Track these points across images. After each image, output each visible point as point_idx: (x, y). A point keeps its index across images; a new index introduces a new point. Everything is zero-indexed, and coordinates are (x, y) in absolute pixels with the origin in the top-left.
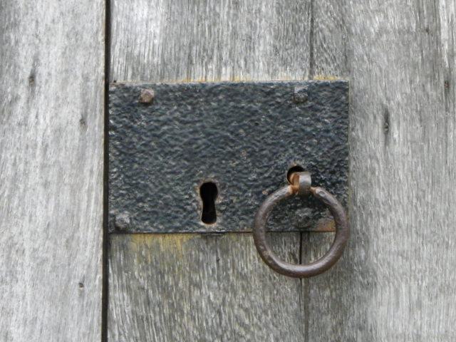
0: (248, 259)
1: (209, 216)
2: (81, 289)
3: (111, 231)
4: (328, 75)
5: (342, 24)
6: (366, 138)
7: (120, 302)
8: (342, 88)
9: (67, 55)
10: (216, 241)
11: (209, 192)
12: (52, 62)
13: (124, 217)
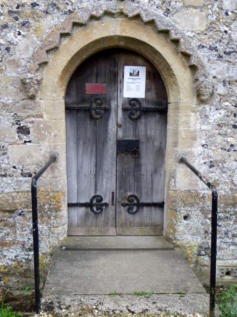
0: (130, 156)
1: (126, 152)
2: (230, 144)
3: (117, 153)
4: (137, 139)
5: (139, 134)
6: (141, 145)
7: (118, 160)
8: (138, 140)
9: (113, 137)
10: (57, 168)
11: (126, 150)
12: (112, 138)
13: (118, 152)
